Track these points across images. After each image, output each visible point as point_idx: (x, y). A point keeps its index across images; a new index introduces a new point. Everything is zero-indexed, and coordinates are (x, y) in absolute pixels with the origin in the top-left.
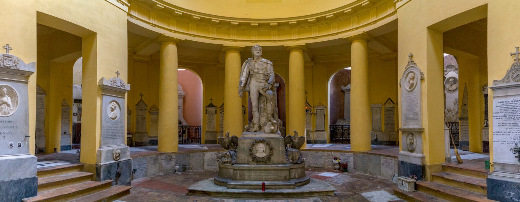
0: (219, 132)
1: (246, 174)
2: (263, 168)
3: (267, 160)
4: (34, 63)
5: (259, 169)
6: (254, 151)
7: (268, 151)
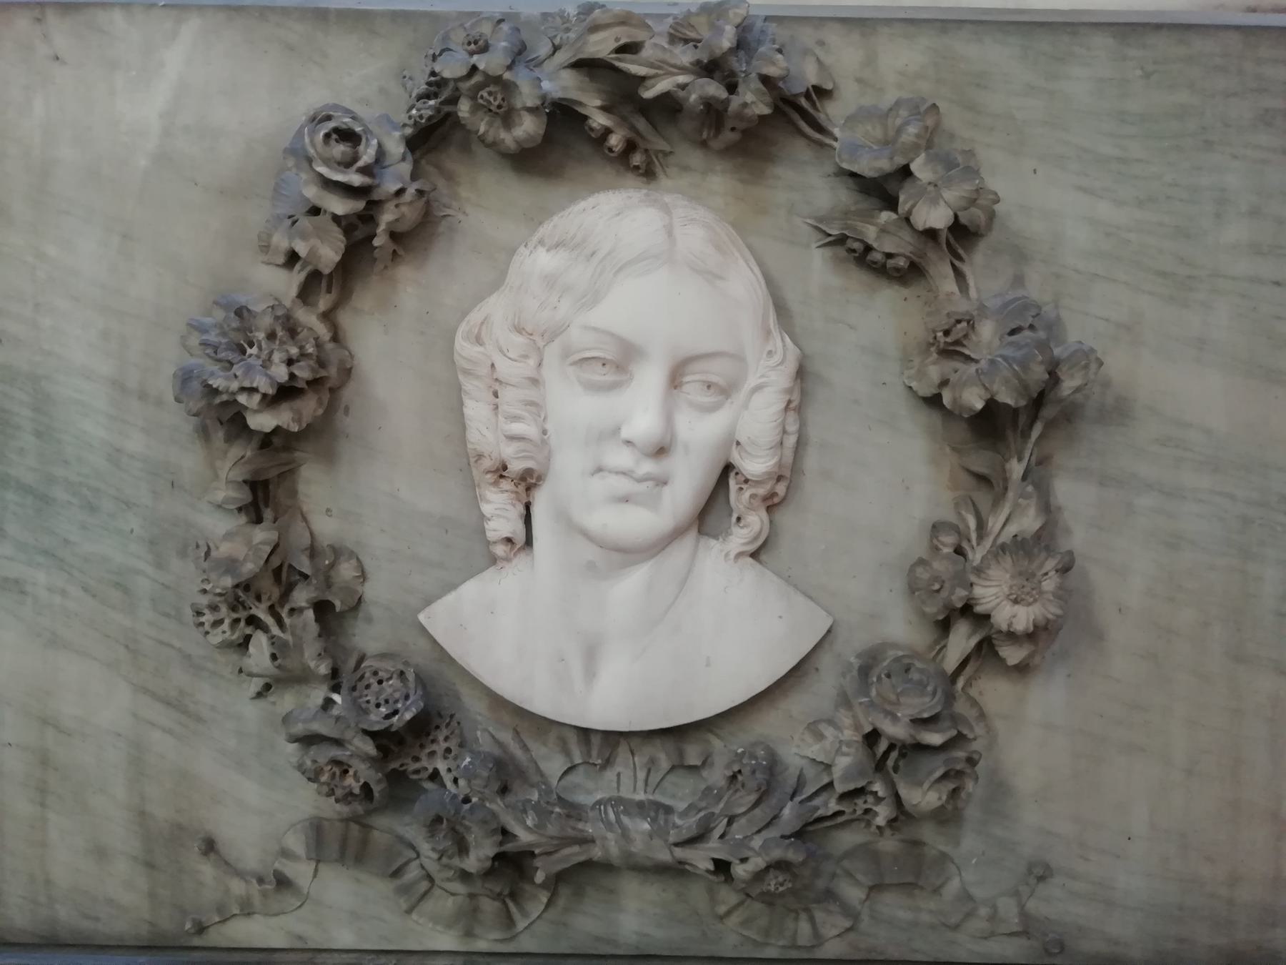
6: (362, 504)
7: (890, 484)
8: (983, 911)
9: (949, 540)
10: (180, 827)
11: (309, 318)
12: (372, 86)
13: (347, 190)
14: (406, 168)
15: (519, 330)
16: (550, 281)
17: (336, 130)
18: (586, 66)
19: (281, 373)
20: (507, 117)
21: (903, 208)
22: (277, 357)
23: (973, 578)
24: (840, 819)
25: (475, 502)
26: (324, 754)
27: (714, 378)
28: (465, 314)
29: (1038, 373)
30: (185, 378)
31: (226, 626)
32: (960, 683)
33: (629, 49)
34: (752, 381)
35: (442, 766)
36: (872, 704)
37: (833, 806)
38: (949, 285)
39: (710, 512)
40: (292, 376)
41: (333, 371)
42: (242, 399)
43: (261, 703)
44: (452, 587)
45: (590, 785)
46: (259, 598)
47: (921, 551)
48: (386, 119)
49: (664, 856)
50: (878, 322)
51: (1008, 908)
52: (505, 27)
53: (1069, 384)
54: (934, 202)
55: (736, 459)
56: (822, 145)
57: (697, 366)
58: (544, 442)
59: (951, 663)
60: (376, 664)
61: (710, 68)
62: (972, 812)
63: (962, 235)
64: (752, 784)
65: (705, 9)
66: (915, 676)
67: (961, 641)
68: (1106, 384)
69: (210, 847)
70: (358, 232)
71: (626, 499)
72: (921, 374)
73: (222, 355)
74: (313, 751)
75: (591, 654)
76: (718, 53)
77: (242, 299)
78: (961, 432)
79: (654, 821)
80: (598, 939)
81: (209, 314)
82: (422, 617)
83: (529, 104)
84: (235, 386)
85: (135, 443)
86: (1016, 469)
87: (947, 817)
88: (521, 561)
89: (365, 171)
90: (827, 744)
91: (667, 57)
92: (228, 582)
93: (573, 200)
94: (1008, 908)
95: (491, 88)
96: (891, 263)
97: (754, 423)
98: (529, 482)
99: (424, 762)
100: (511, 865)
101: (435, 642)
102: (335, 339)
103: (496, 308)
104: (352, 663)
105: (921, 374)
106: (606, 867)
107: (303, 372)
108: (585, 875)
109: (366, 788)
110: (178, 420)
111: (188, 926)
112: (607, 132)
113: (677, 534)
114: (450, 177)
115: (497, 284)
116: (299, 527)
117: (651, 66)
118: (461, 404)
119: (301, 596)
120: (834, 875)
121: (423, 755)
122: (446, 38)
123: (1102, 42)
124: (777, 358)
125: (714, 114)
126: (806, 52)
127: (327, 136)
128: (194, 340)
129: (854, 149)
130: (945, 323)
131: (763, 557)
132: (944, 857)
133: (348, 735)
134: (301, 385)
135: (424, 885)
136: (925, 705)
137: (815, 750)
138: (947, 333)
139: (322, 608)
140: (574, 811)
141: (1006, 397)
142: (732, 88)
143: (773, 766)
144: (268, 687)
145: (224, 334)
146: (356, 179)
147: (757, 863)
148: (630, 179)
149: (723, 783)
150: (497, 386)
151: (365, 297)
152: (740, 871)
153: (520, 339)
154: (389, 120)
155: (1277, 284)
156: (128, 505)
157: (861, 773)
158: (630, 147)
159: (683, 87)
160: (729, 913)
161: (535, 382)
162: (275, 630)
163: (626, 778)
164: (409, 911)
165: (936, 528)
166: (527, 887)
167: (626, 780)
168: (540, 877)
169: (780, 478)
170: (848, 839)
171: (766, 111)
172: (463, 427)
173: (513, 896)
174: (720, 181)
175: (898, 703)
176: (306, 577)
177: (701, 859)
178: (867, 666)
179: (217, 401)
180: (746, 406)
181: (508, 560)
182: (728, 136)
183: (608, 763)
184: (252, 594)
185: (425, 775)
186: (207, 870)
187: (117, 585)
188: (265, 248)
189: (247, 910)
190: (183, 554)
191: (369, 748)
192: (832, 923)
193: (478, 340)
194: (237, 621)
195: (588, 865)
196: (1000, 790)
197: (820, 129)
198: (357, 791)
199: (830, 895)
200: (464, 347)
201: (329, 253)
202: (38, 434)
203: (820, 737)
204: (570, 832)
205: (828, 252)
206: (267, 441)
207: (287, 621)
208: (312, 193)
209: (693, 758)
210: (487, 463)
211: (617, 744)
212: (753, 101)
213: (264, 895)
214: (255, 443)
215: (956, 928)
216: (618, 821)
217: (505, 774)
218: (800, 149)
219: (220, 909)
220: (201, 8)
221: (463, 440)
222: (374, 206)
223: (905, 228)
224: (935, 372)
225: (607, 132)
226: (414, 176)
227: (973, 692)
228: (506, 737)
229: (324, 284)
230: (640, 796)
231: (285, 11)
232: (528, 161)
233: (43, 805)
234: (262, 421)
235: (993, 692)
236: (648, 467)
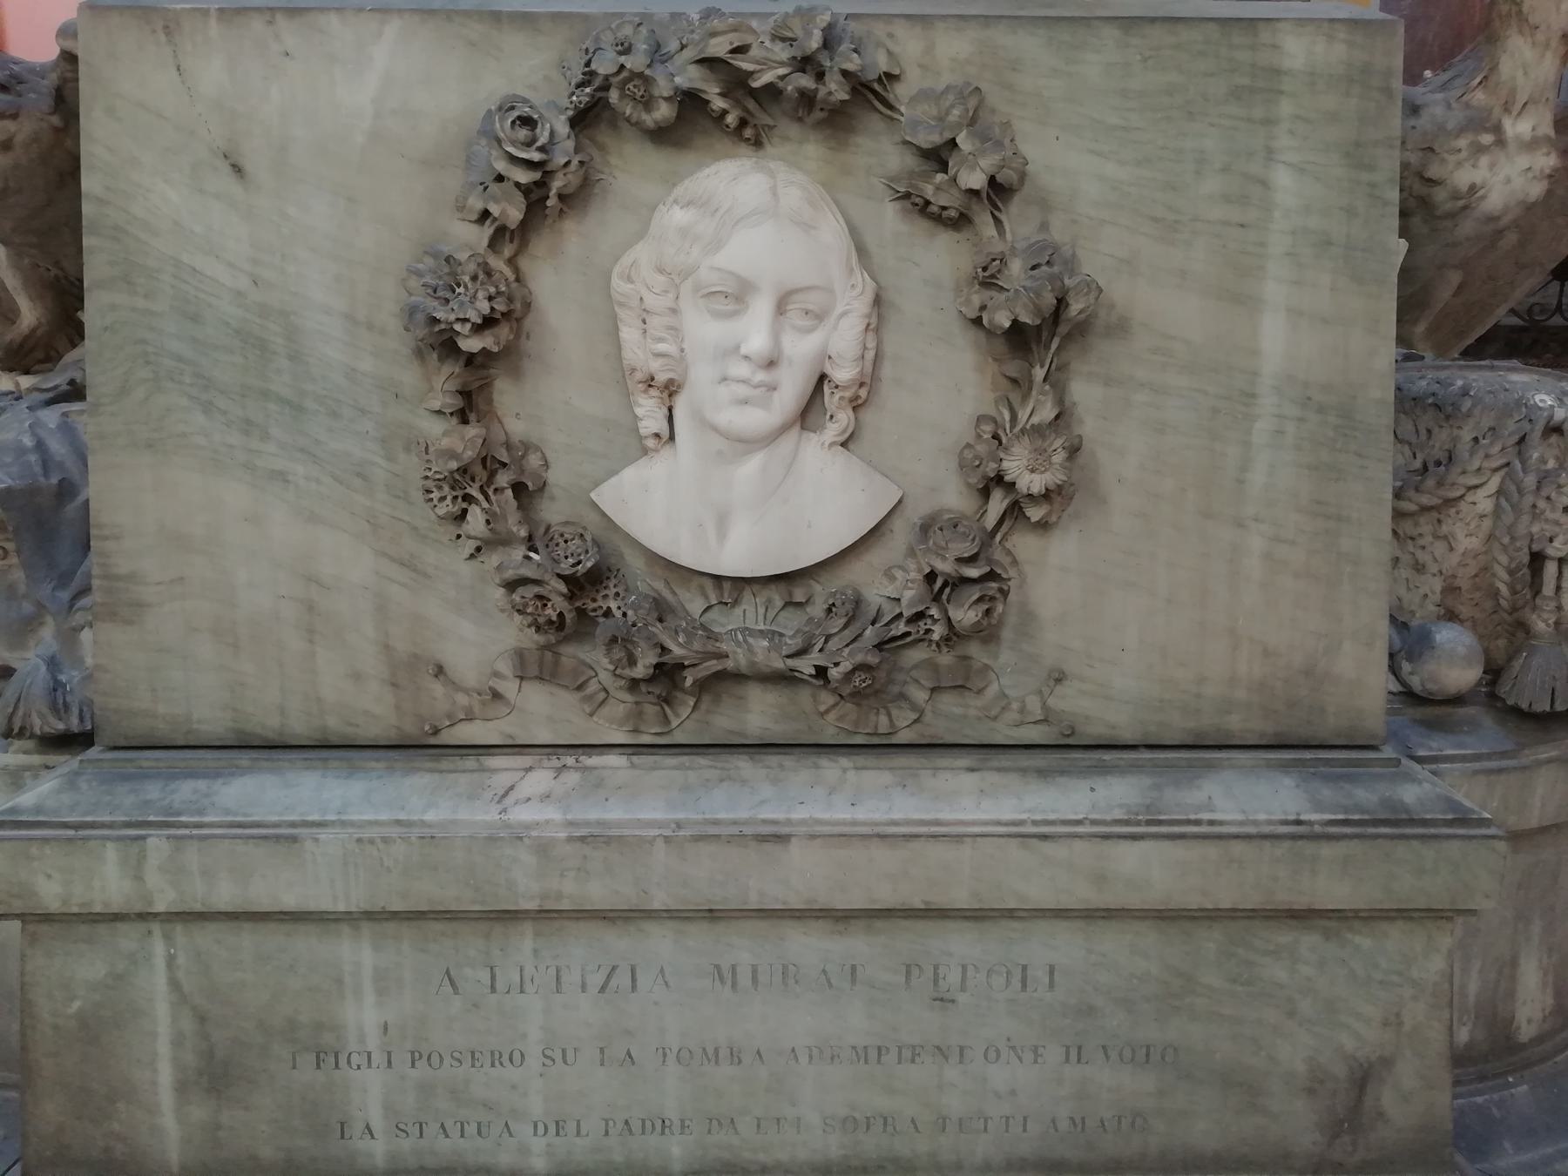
0: (32, 736)
1: (363, 1018)
2: (802, 876)
3: (893, 655)
4: (150, 903)
5: (876, 879)
6: (545, 408)
7: (946, 388)
8: (1015, 706)
9: (988, 429)
10: (415, 656)
11: (498, 264)
12: (536, 74)
13: (529, 164)
14: (570, 144)
15: (661, 271)
16: (684, 232)
17: (519, 118)
18: (708, 62)
19: (485, 307)
20: (647, 103)
21: (952, 172)
22: (481, 295)
23: (1002, 455)
24: (909, 639)
25: (630, 407)
26: (530, 591)
27: (811, 307)
28: (617, 259)
29: (1049, 300)
30: (412, 311)
31: (448, 501)
32: (998, 537)
33: (740, 50)
34: (839, 309)
35: (613, 605)
36: (928, 549)
37: (901, 628)
38: (990, 231)
39: (809, 412)
40: (492, 309)
41: (518, 306)
42: (457, 327)
43: (473, 563)
44: (614, 473)
45: (723, 620)
46: (473, 480)
47: (969, 437)
48: (553, 105)
49: (779, 664)
50: (939, 259)
51: (1034, 705)
52: (644, 30)
53: (1075, 307)
54: (973, 168)
55: (829, 370)
56: (892, 119)
57: (795, 297)
58: (682, 359)
59: (991, 520)
60: (562, 529)
61: (805, 63)
62: (1007, 634)
63: (998, 191)
64: (842, 611)
65: (799, 11)
66: (961, 529)
67: (998, 503)
68: (1112, 307)
69: (440, 671)
70: (535, 197)
71: (745, 402)
72: (968, 301)
73: (440, 293)
74: (520, 590)
75: (722, 522)
76: (809, 52)
77: (446, 249)
78: (1001, 346)
79: (771, 640)
80: (732, 732)
81: (420, 261)
82: (593, 495)
83: (666, 94)
84: (452, 317)
85: (366, 365)
86: (1039, 373)
87: (987, 633)
88: (666, 452)
89: (542, 149)
90: (898, 583)
91: (769, 55)
92: (454, 465)
93: (700, 166)
94: (1034, 705)
95: (636, 82)
96: (945, 214)
97: (841, 340)
98: (671, 390)
99: (600, 603)
100: (667, 673)
101: (604, 515)
102: (518, 280)
103: (642, 254)
104: (542, 530)
105: (968, 301)
106: (738, 677)
107: (501, 307)
108: (723, 681)
109: (561, 615)
110: (399, 342)
111: (427, 728)
112: (725, 112)
113: (784, 429)
114: (602, 148)
115: (641, 234)
116: (496, 427)
117: (758, 63)
118: (617, 329)
119: (503, 479)
120: (905, 682)
121: (599, 597)
122: (597, 39)
123: (1110, 33)
124: (859, 290)
125: (807, 99)
126: (879, 44)
127: (513, 122)
128: (414, 283)
129: (915, 124)
130: (982, 260)
131: (851, 446)
132: (987, 667)
133: (547, 577)
134: (498, 316)
135: (602, 695)
136: (967, 549)
137: (890, 591)
138: (985, 269)
139: (518, 488)
140: (712, 636)
141: (1025, 318)
142: (820, 76)
143: (858, 602)
144: (478, 549)
145: (440, 278)
146: (536, 156)
147: (846, 666)
148: (744, 149)
149: (822, 615)
150: (645, 315)
151: (540, 245)
152: (834, 673)
153: (662, 278)
154: (556, 106)
155: (1242, 226)
156: (363, 411)
157: (921, 601)
158: (743, 123)
159: (782, 78)
160: (827, 711)
161: (674, 311)
162: (485, 505)
163: (751, 611)
164: (591, 715)
165: (980, 419)
166: (679, 695)
167: (750, 614)
168: (689, 682)
169: (862, 385)
170: (916, 655)
171: (847, 97)
172: (619, 348)
173: (667, 701)
174: (813, 149)
175: (946, 549)
176: (504, 465)
177: (806, 666)
178: (926, 528)
179: (437, 329)
180: (835, 328)
181: (656, 451)
182: (818, 115)
183: (736, 602)
184: (468, 478)
185: (600, 612)
186: (438, 689)
187: (359, 475)
188: (461, 208)
189: (470, 718)
190: (407, 449)
191: (563, 588)
192: (903, 717)
193: (630, 280)
194: (455, 498)
195: (721, 676)
196: (1028, 617)
197: (891, 107)
198: (554, 618)
199: (902, 696)
200: (618, 284)
201: (513, 213)
202: (291, 358)
203: (892, 579)
204: (710, 648)
205: (898, 205)
206: (470, 359)
207: (493, 497)
208: (501, 166)
209: (799, 596)
210: (639, 376)
211: (741, 591)
212: (834, 89)
213: (483, 703)
214: (462, 362)
215: (995, 718)
216: (745, 641)
217: (662, 610)
218: (874, 122)
219: (449, 716)
220: (400, 11)
221: (620, 358)
222: (548, 174)
223: (960, 189)
224: (976, 300)
225: (725, 112)
226: (577, 150)
227: (1008, 545)
228: (659, 586)
229: (508, 236)
230: (762, 627)
231: (467, 13)
232: (661, 136)
233: (311, 641)
234: (471, 344)
235: (1023, 544)
236: (761, 376)
